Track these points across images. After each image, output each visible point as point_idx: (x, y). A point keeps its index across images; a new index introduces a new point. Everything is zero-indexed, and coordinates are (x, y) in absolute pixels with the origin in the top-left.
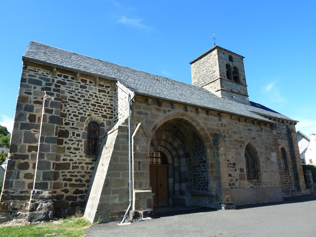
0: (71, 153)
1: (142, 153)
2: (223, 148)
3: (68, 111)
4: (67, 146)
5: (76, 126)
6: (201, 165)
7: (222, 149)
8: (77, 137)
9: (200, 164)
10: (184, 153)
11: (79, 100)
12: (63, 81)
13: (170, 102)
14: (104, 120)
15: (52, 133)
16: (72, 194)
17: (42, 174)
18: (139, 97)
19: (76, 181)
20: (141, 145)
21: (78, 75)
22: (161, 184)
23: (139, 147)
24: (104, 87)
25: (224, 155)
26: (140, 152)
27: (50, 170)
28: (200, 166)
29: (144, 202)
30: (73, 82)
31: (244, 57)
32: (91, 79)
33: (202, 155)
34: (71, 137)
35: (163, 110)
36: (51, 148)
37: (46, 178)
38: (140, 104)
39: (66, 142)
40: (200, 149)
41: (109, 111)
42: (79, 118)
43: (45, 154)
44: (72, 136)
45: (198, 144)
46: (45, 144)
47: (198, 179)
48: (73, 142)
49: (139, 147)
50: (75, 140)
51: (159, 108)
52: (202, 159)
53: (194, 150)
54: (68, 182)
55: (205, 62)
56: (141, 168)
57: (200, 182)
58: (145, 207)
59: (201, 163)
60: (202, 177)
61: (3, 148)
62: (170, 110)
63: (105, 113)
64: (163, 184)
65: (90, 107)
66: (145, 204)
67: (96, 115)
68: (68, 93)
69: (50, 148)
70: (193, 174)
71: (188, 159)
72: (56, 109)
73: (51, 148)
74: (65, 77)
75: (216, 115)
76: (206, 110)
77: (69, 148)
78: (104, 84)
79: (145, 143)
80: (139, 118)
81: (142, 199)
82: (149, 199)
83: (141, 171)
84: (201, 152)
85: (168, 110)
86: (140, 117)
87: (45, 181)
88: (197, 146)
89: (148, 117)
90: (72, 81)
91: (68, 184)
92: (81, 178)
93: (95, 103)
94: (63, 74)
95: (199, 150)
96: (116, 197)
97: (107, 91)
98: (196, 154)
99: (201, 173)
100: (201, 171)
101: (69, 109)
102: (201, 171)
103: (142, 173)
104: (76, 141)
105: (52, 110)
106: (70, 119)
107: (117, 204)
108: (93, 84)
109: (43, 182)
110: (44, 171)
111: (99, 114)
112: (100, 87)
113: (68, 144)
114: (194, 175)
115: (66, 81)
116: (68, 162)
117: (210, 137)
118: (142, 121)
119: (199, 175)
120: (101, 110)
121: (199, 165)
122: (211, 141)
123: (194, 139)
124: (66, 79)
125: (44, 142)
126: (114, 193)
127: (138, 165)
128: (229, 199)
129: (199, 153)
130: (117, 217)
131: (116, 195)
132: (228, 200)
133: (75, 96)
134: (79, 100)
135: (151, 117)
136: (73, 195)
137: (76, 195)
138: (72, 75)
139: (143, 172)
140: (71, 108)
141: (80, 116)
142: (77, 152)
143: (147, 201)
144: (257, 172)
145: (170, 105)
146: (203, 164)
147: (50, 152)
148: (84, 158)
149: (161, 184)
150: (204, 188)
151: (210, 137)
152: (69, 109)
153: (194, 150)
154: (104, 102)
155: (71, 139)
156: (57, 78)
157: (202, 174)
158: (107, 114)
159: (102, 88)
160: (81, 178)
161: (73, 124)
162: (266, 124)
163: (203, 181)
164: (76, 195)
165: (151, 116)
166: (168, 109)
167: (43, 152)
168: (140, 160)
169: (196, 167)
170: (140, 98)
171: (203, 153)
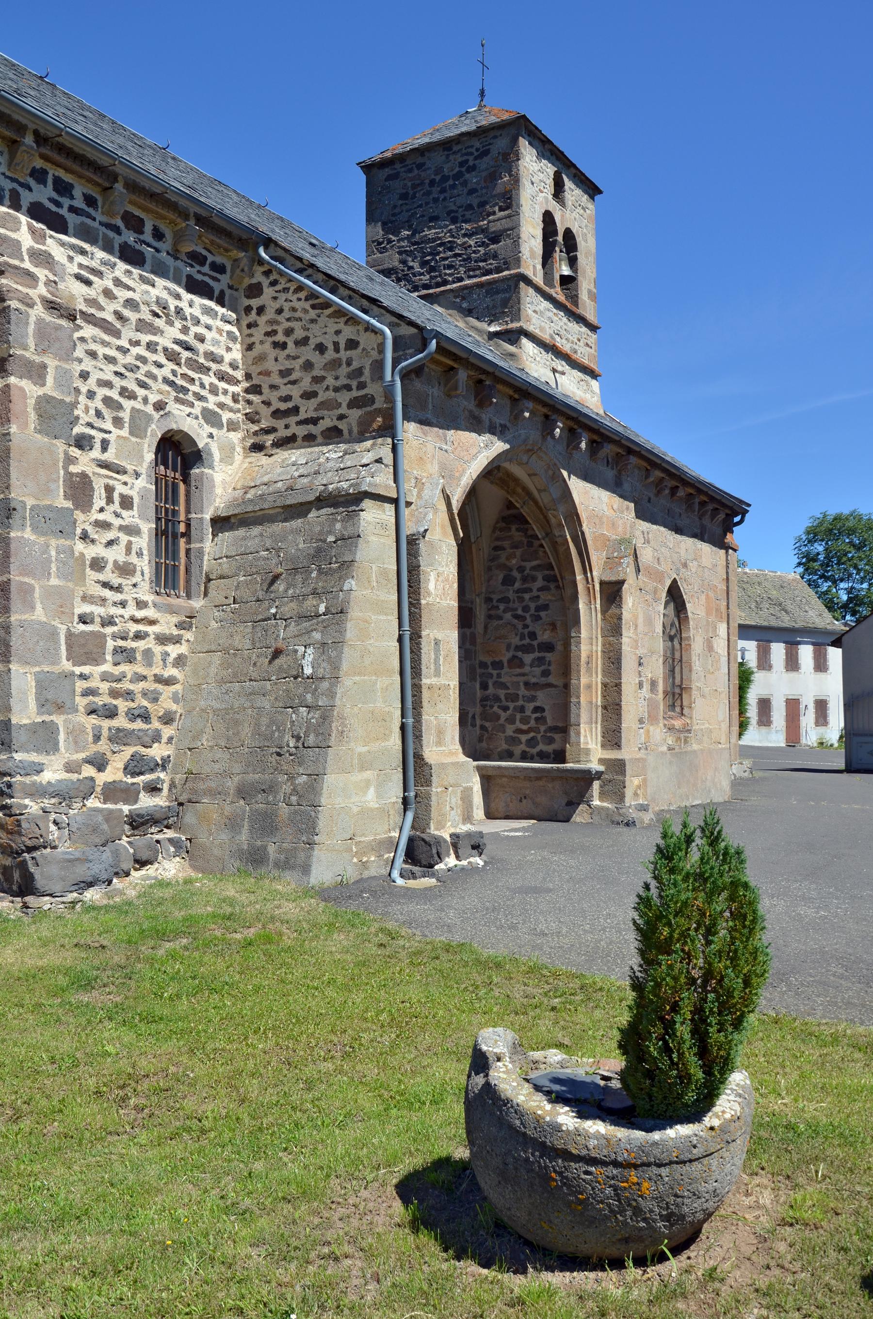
0: (106, 585)
3: (84, 375)
4: (91, 552)
5: (117, 456)
6: (528, 658)
8: (125, 513)
9: (520, 654)
11: (118, 325)
12: (53, 208)
13: (511, 392)
14: (211, 436)
15: (53, 486)
16: (120, 776)
17: (34, 684)
19: (133, 716)
21: (119, 186)
24: (206, 269)
27: (58, 664)
28: (521, 664)
30: (94, 219)
31: (600, 192)
32: (162, 217)
33: (538, 618)
34: (102, 510)
35: (487, 423)
36: (53, 559)
37: (47, 700)
39: (85, 537)
40: (527, 596)
41: (225, 392)
42: (126, 415)
43: (37, 586)
44: (103, 503)
45: (515, 574)
46: (33, 537)
47: (503, 715)
48: (110, 535)
50: (117, 522)
51: (476, 411)
52: (533, 635)
53: (495, 597)
54: (106, 724)
55: (445, 178)
57: (519, 725)
59: (527, 649)
60: (530, 706)
61: (666, 604)
63: (212, 402)
65: (160, 366)
67: (182, 407)
68: (78, 277)
69: (51, 562)
70: (479, 694)
72: (57, 363)
73: (53, 559)
74: (63, 188)
76: (595, 437)
77: (97, 564)
78: (204, 252)
81: (450, 789)
84: (533, 606)
87: (47, 718)
88: (508, 581)
90: (89, 216)
91: (105, 733)
92: (145, 703)
93: (177, 348)
94: (53, 172)
95: (521, 600)
96: (368, 783)
97: (217, 287)
98: (504, 611)
99: (522, 691)
100: (526, 684)
101: (88, 364)
102: (526, 684)
104: (121, 528)
105: (44, 367)
106: (91, 417)
107: (372, 810)
108: (165, 246)
109: (39, 720)
110: (37, 669)
111: (192, 405)
112: (192, 266)
113: (93, 541)
114: (484, 699)
115: (64, 212)
116: (95, 627)
119: (514, 698)
120: (197, 383)
121: (514, 657)
123: (496, 548)
124: (66, 202)
125: (29, 529)
126: (362, 768)
127: (433, 656)
129: (520, 612)
130: (373, 859)
131: (368, 774)
133: (102, 300)
134: (118, 325)
136: (125, 779)
137: (135, 780)
138: (89, 180)
140: (94, 362)
141: (128, 404)
142: (126, 582)
144: (681, 695)
145: (508, 402)
146: (537, 654)
147: (54, 581)
148: (149, 613)
150: (534, 751)
152: (88, 364)
153: (495, 597)
154: (207, 347)
155: (101, 517)
156: (30, 190)
157: (527, 693)
158: (221, 405)
159: (199, 272)
160: (145, 703)
161: (104, 449)
163: (533, 723)
164: (135, 780)
167: (26, 580)
168: (440, 636)
169: (498, 665)
171: (543, 614)
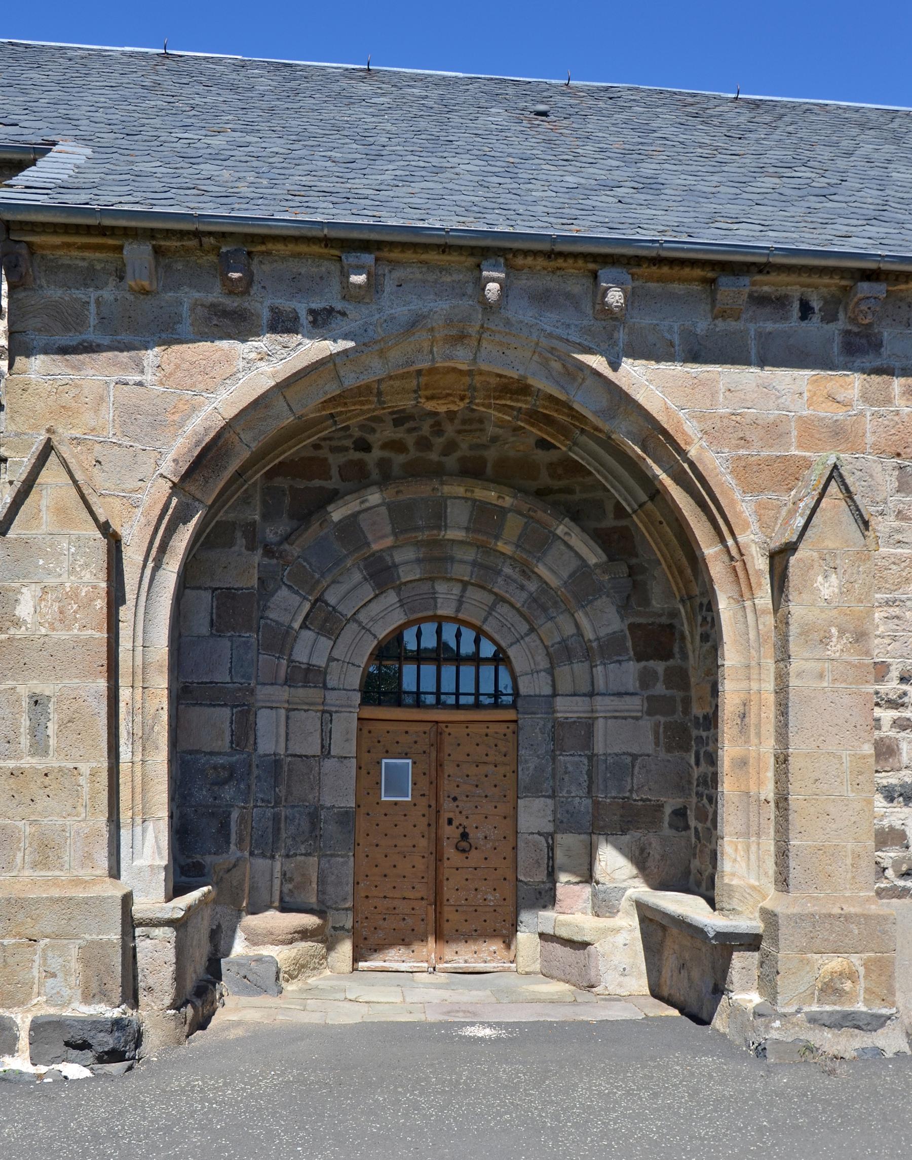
1: (62, 634)
2: (833, 578)
7: (827, 587)
10: (632, 627)
18: (57, 240)
20: (52, 581)
22: (464, 836)
23: (41, 599)
25: (842, 632)
26: (43, 631)
29: (55, 964)
38: (79, 294)
49: (41, 599)
56: (52, 742)
58: (66, 992)
62: (330, 311)
64: (481, 835)
66: (67, 973)
71: (659, 667)
75: (816, 305)
79: (86, 565)
80: (73, 392)
81: (43, 942)
82: (100, 944)
83: (52, 762)
85: (312, 312)
86: (76, 386)
89: (140, 384)
103: (61, 769)
117: (738, 496)
118: (96, 411)
122: (746, 526)
127: (25, 722)
128: (848, 985)
132: (839, 993)
135: (168, 376)
139: (71, 766)
143: (86, 961)
149: (464, 836)
151: (738, 496)
162: (713, 281)
165: (168, 369)
166: (314, 306)
170: (68, 246)
